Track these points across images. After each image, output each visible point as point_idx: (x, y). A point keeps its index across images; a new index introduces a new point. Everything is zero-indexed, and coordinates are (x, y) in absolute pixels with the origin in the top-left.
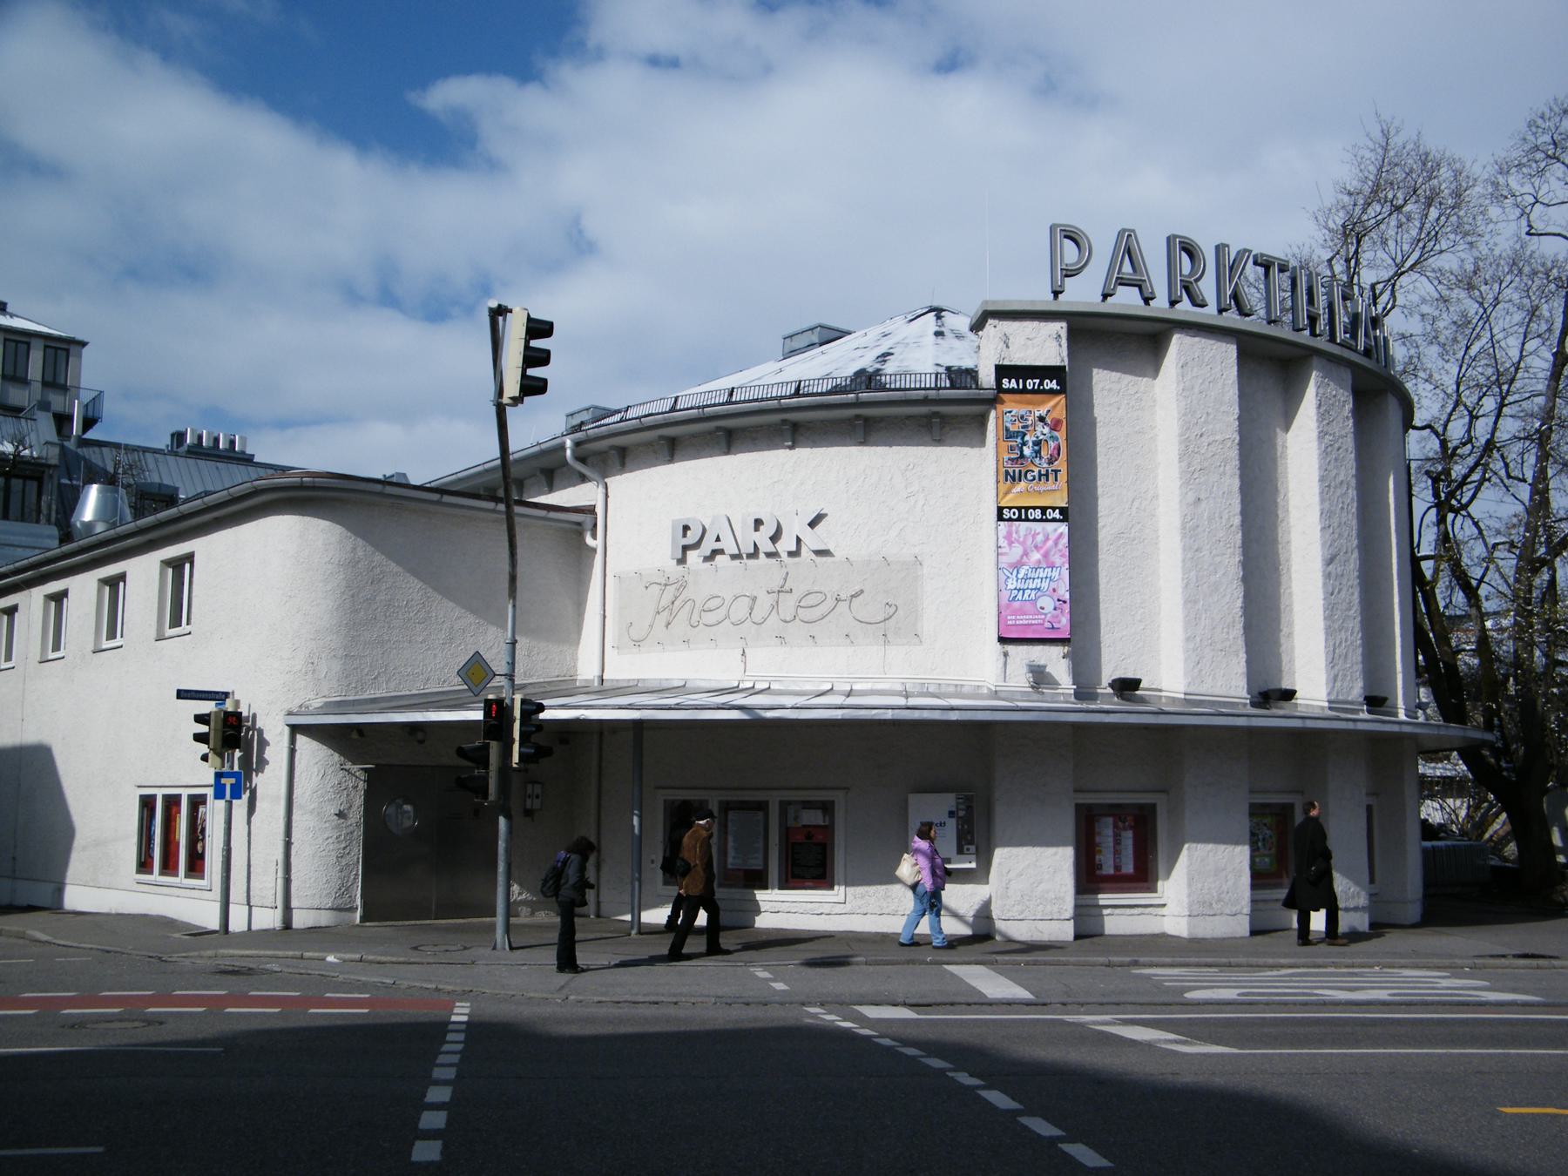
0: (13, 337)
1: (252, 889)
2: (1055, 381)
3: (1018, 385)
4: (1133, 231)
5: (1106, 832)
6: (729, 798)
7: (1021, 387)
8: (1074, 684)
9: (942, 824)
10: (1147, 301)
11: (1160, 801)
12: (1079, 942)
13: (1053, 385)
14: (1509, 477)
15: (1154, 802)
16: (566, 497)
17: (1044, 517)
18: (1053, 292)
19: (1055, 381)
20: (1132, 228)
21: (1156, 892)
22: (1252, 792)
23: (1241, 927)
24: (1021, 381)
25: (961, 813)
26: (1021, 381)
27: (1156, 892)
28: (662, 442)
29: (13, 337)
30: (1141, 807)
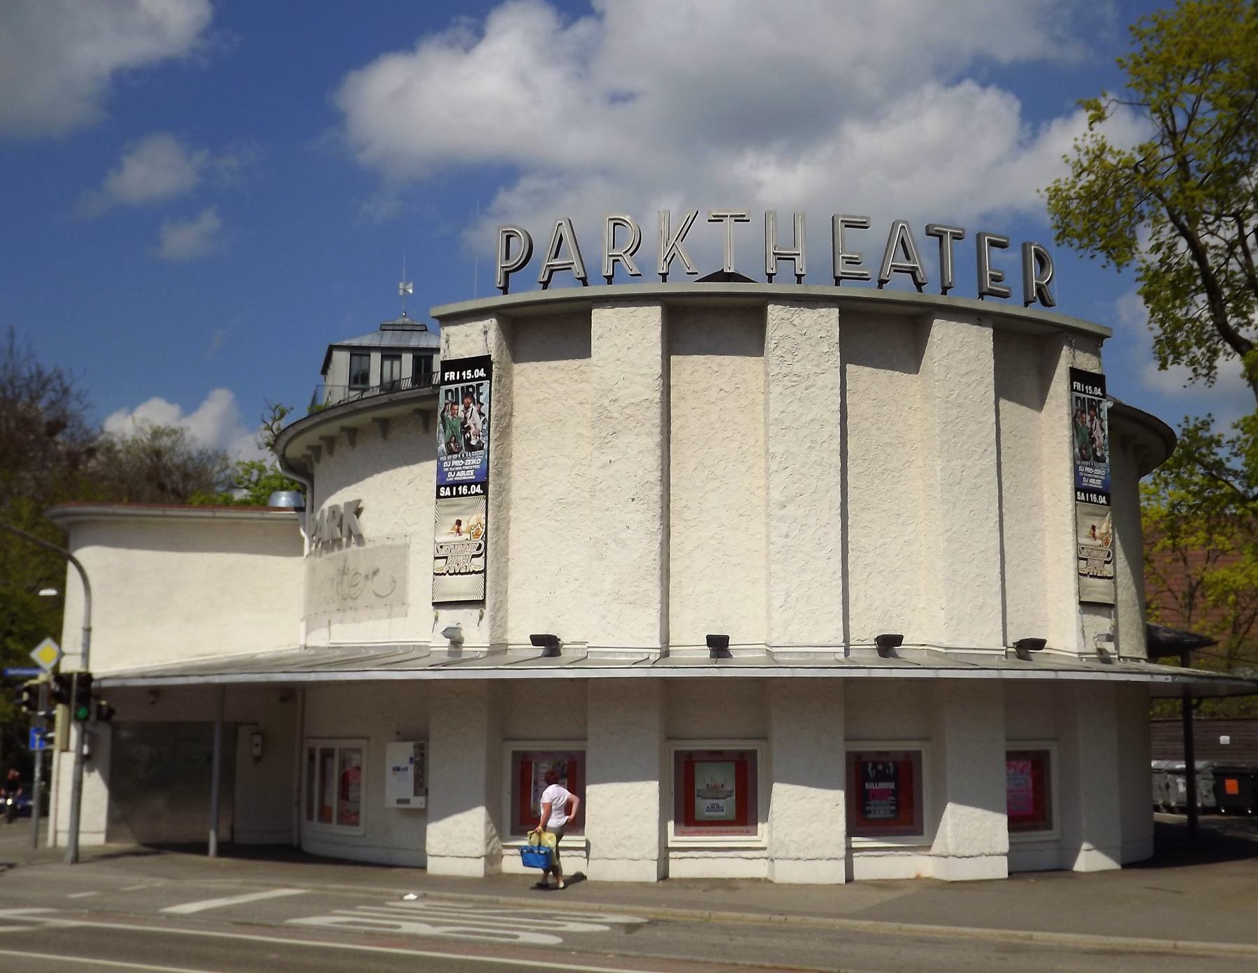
0: (357, 352)
1: (367, 869)
2: (482, 370)
3: (456, 376)
4: (906, 222)
5: (706, 777)
6: (744, 748)
7: (458, 378)
8: (844, 642)
9: (406, 769)
10: (919, 286)
11: (1053, 748)
12: (1019, 885)
13: (482, 373)
14: (798, 440)
15: (919, 749)
16: (1245, 469)
17: (469, 493)
18: (878, 282)
19: (482, 370)
20: (906, 220)
21: (756, 835)
22: (1008, 740)
23: (1000, 868)
24: (458, 373)
25: (417, 759)
26: (458, 373)
27: (756, 835)
28: (376, 424)
29: (357, 352)
30: (742, 754)
